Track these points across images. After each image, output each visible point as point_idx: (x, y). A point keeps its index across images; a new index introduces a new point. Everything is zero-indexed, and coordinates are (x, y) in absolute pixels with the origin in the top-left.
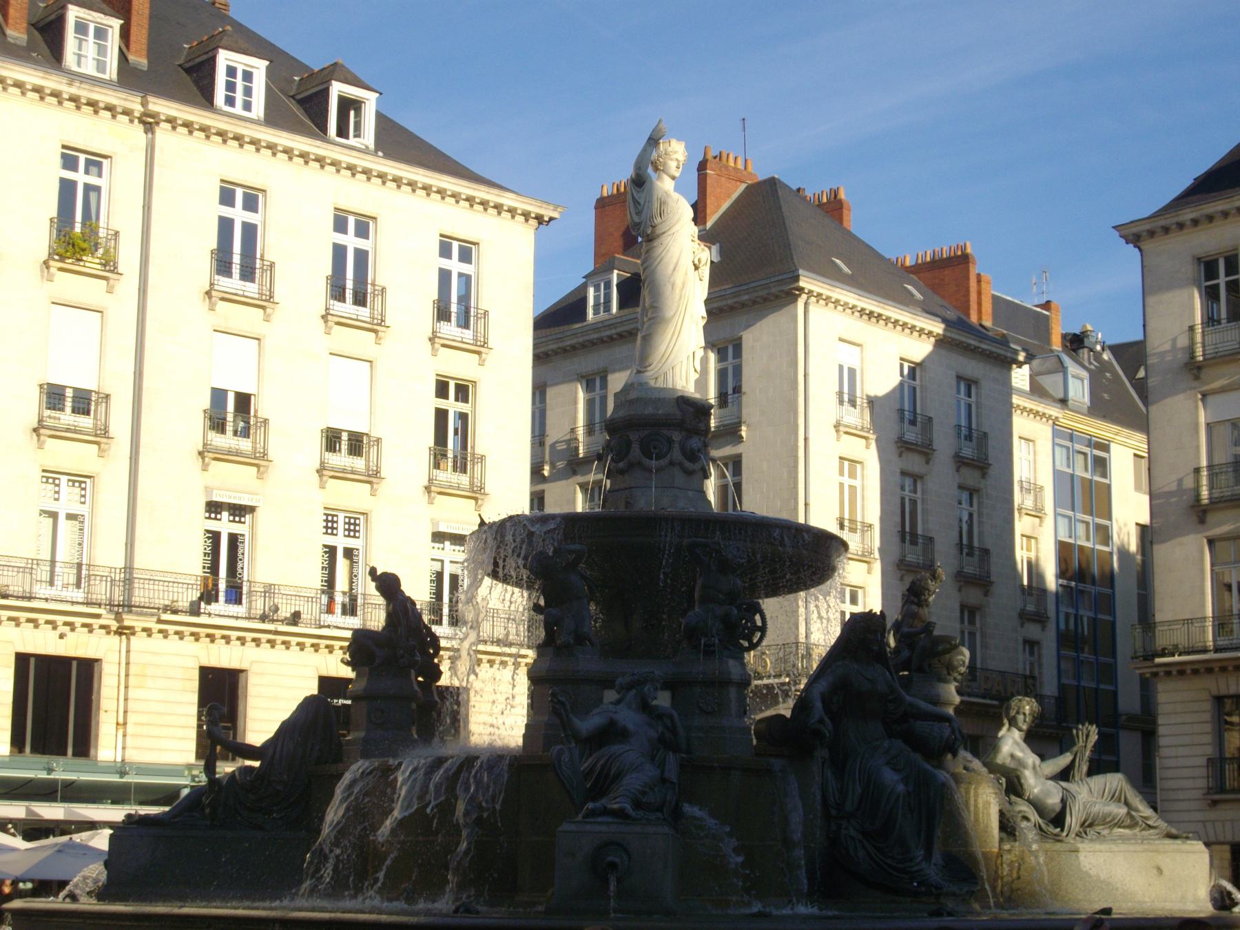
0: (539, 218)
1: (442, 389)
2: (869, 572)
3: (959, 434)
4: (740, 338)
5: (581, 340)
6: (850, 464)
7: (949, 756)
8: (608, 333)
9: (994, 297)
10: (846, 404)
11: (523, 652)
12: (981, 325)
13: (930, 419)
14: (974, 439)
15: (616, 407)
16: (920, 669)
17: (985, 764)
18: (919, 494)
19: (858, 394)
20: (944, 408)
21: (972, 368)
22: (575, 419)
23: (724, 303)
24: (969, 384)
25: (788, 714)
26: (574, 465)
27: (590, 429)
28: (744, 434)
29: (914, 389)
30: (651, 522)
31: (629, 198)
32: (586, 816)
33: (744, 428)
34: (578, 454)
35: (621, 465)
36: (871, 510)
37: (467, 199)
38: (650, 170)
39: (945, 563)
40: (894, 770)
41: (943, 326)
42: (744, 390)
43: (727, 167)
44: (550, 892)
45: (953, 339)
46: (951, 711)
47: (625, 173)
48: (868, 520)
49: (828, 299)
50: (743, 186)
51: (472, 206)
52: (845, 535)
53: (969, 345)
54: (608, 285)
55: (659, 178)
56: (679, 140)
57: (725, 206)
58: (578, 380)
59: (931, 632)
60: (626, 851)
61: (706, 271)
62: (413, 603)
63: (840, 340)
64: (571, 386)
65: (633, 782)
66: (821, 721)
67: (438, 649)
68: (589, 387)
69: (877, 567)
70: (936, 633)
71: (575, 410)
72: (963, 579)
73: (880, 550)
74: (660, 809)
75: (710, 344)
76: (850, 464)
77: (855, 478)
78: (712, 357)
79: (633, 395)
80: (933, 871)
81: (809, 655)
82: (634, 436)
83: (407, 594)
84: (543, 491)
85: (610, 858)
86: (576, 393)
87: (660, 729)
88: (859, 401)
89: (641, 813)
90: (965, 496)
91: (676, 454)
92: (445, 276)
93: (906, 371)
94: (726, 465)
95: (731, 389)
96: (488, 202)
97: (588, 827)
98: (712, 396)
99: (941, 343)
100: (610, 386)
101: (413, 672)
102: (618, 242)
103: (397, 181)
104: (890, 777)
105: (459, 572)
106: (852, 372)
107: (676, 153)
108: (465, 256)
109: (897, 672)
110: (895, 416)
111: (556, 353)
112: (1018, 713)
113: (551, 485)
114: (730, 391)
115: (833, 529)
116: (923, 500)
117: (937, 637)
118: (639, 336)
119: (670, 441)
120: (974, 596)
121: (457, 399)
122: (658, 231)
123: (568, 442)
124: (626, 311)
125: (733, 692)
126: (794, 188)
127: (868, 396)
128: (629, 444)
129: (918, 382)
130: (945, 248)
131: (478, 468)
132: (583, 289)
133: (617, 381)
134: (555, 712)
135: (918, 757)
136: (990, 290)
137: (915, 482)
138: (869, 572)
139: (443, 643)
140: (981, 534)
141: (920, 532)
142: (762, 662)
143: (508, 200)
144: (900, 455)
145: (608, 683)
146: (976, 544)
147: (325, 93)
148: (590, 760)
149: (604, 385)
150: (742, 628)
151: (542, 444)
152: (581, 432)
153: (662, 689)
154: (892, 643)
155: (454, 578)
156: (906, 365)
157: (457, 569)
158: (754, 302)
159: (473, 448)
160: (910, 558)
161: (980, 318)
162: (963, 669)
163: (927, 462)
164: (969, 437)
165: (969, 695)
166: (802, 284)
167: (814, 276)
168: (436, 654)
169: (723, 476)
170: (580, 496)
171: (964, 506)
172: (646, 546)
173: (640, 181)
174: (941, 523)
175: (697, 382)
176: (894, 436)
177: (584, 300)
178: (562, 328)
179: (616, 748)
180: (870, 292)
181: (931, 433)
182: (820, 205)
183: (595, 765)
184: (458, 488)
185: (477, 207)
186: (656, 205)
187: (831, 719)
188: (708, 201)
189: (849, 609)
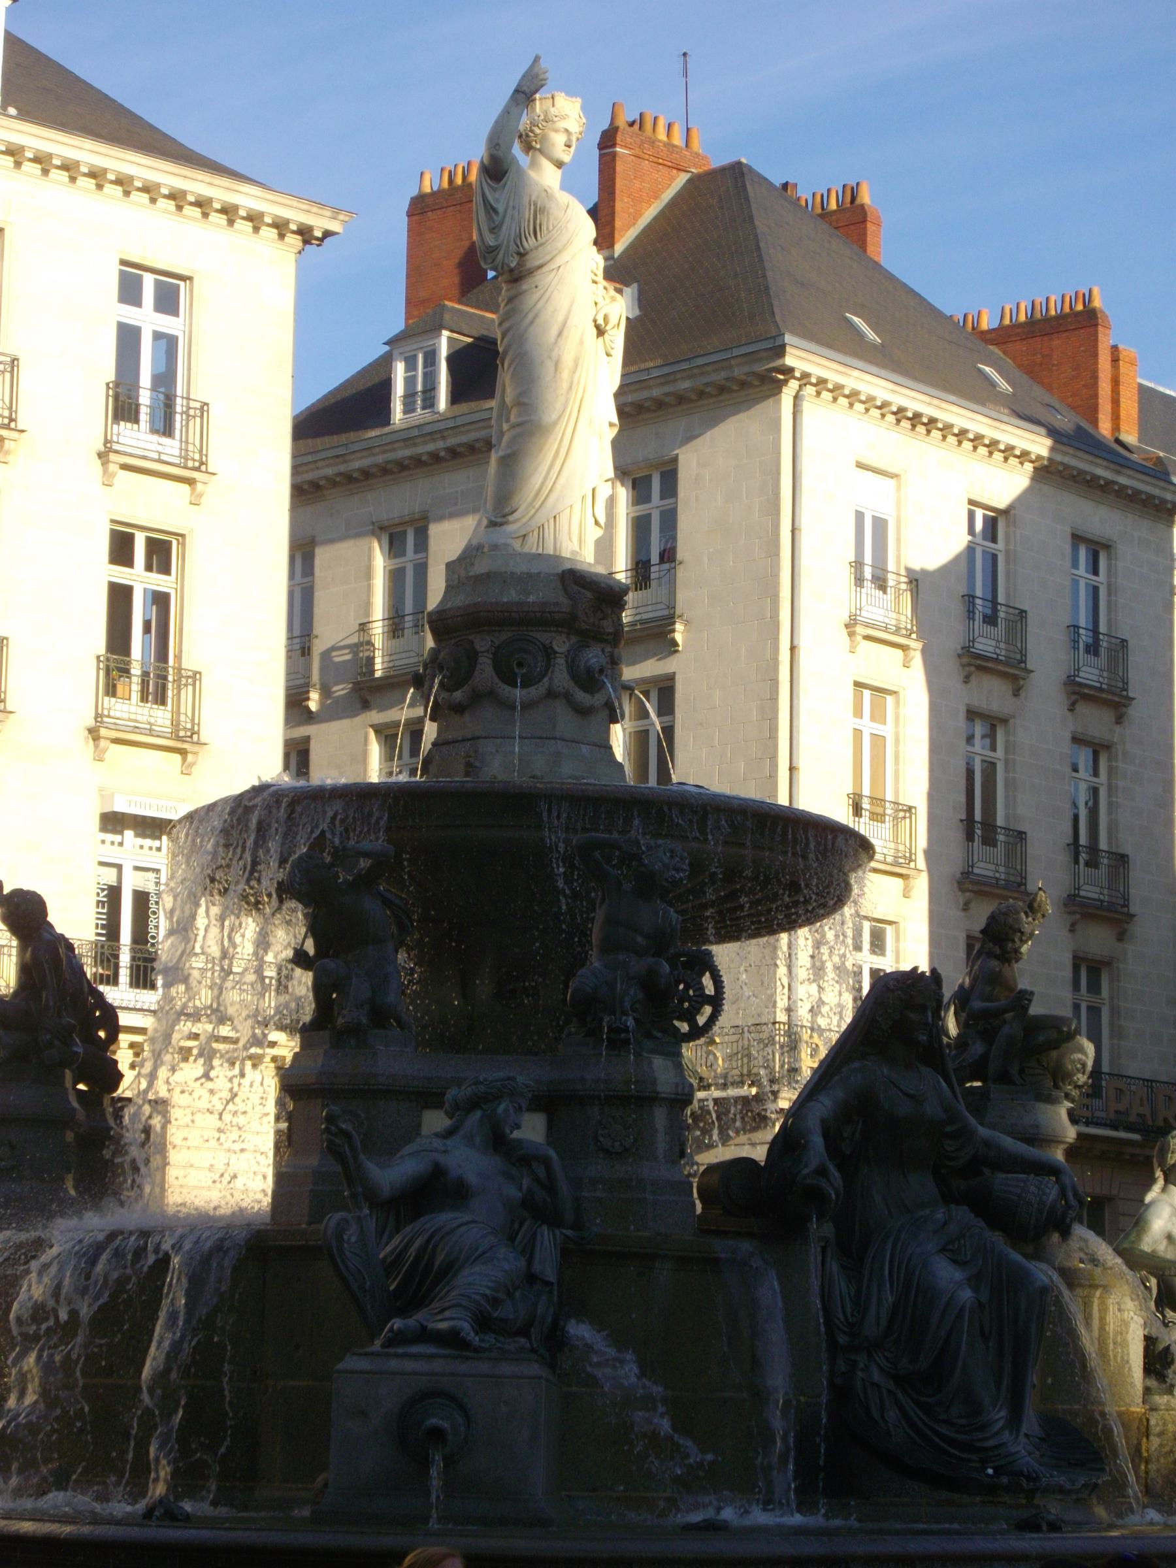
0: (305, 233)
1: (121, 548)
2: (906, 895)
3: (1075, 641)
4: (675, 460)
5: (380, 459)
6: (873, 695)
7: (1056, 1237)
8: (431, 447)
9: (1141, 388)
10: (867, 584)
11: (275, 1035)
12: (1118, 441)
13: (1022, 613)
14: (1102, 651)
15: (450, 589)
16: (1004, 1077)
17: (1119, 1252)
18: (1000, 752)
19: (891, 566)
20: (1049, 595)
21: (1101, 519)
22: (367, 606)
23: (645, 394)
24: (1095, 549)
25: (759, 1154)
26: (366, 692)
27: (395, 625)
28: (678, 637)
29: (994, 557)
30: (520, 803)
31: (477, 199)
32: (389, 1343)
33: (679, 627)
34: (373, 671)
35: (458, 695)
36: (912, 779)
37: (172, 196)
38: (517, 150)
39: (1048, 876)
40: (955, 1262)
41: (1048, 442)
42: (680, 555)
43: (653, 142)
44: (320, 1479)
45: (1067, 467)
46: (1059, 1155)
47: (476, 153)
48: (906, 800)
49: (837, 389)
50: (683, 178)
51: (180, 208)
52: (863, 826)
53: (1096, 478)
54: (431, 358)
55: (534, 164)
56: (570, 94)
57: (649, 214)
58: (373, 533)
59: (1025, 1009)
60: (462, 1407)
61: (617, 338)
62: (70, 947)
63: (860, 465)
64: (362, 542)
65: (476, 1280)
66: (822, 1171)
67: (114, 1030)
68: (395, 546)
69: (921, 884)
70: (1035, 1010)
71: (366, 587)
72: (1079, 909)
73: (928, 854)
74: (524, 1332)
75: (622, 472)
76: (873, 695)
77: (884, 722)
78: (623, 494)
79: (481, 567)
80: (1022, 1449)
81: (793, 1045)
82: (483, 643)
83: (59, 929)
84: (307, 739)
85: (434, 1421)
86: (370, 558)
87: (526, 1182)
88: (891, 580)
89: (490, 1339)
90: (1084, 757)
91: (560, 677)
92: (128, 337)
93: (979, 525)
94: (646, 694)
95: (656, 549)
96: (210, 201)
97: (394, 1364)
98: (621, 568)
99: (1045, 472)
100: (433, 546)
101: (68, 1075)
102: (450, 278)
103: (42, 160)
104: (947, 1274)
105: (151, 888)
106: (880, 525)
107: (567, 118)
108: (167, 301)
109: (961, 1083)
110: (957, 609)
111: (333, 483)
113: (323, 727)
114: (655, 559)
115: (841, 814)
116: (1007, 761)
117: (1037, 1018)
118: (494, 457)
119: (549, 653)
120: (1098, 940)
121: (149, 568)
122: (531, 262)
123: (355, 648)
124: (463, 408)
125: (660, 1116)
126: (778, 182)
127: (908, 570)
129: (1001, 545)
130: (1050, 292)
131: (187, 694)
132: (384, 364)
133: (450, 538)
134: (333, 1150)
135: (998, 1239)
136: (1136, 377)
137: (993, 727)
138: (906, 895)
139: (124, 1019)
140: (1112, 828)
141: (1000, 822)
142: (710, 1061)
143: (247, 198)
144: (967, 679)
145: (430, 1098)
146: (1103, 845)
148: (395, 1241)
149: (422, 543)
150: (677, 998)
151: (306, 651)
152: (378, 631)
153: (529, 1110)
154: (952, 1026)
155: (142, 900)
156: (979, 514)
157: (145, 882)
158: (701, 394)
159: (178, 657)
160: (983, 869)
161: (1116, 428)
162: (1082, 1079)
163: (1016, 693)
164: (1093, 649)
165: (1087, 1124)
166: (789, 361)
167: (813, 346)
168: (113, 1038)
169: (643, 714)
170: (375, 750)
171: (1082, 774)
172: (499, 852)
173: (497, 169)
174: (1040, 808)
175: (598, 543)
176: (954, 643)
177: (386, 385)
178: (343, 438)
179: (444, 1218)
180: (915, 378)
181: (1024, 640)
182: (825, 215)
184: (151, 732)
185: (189, 210)
186: (528, 214)
187: (839, 1167)
188: (619, 205)
189: (868, 961)
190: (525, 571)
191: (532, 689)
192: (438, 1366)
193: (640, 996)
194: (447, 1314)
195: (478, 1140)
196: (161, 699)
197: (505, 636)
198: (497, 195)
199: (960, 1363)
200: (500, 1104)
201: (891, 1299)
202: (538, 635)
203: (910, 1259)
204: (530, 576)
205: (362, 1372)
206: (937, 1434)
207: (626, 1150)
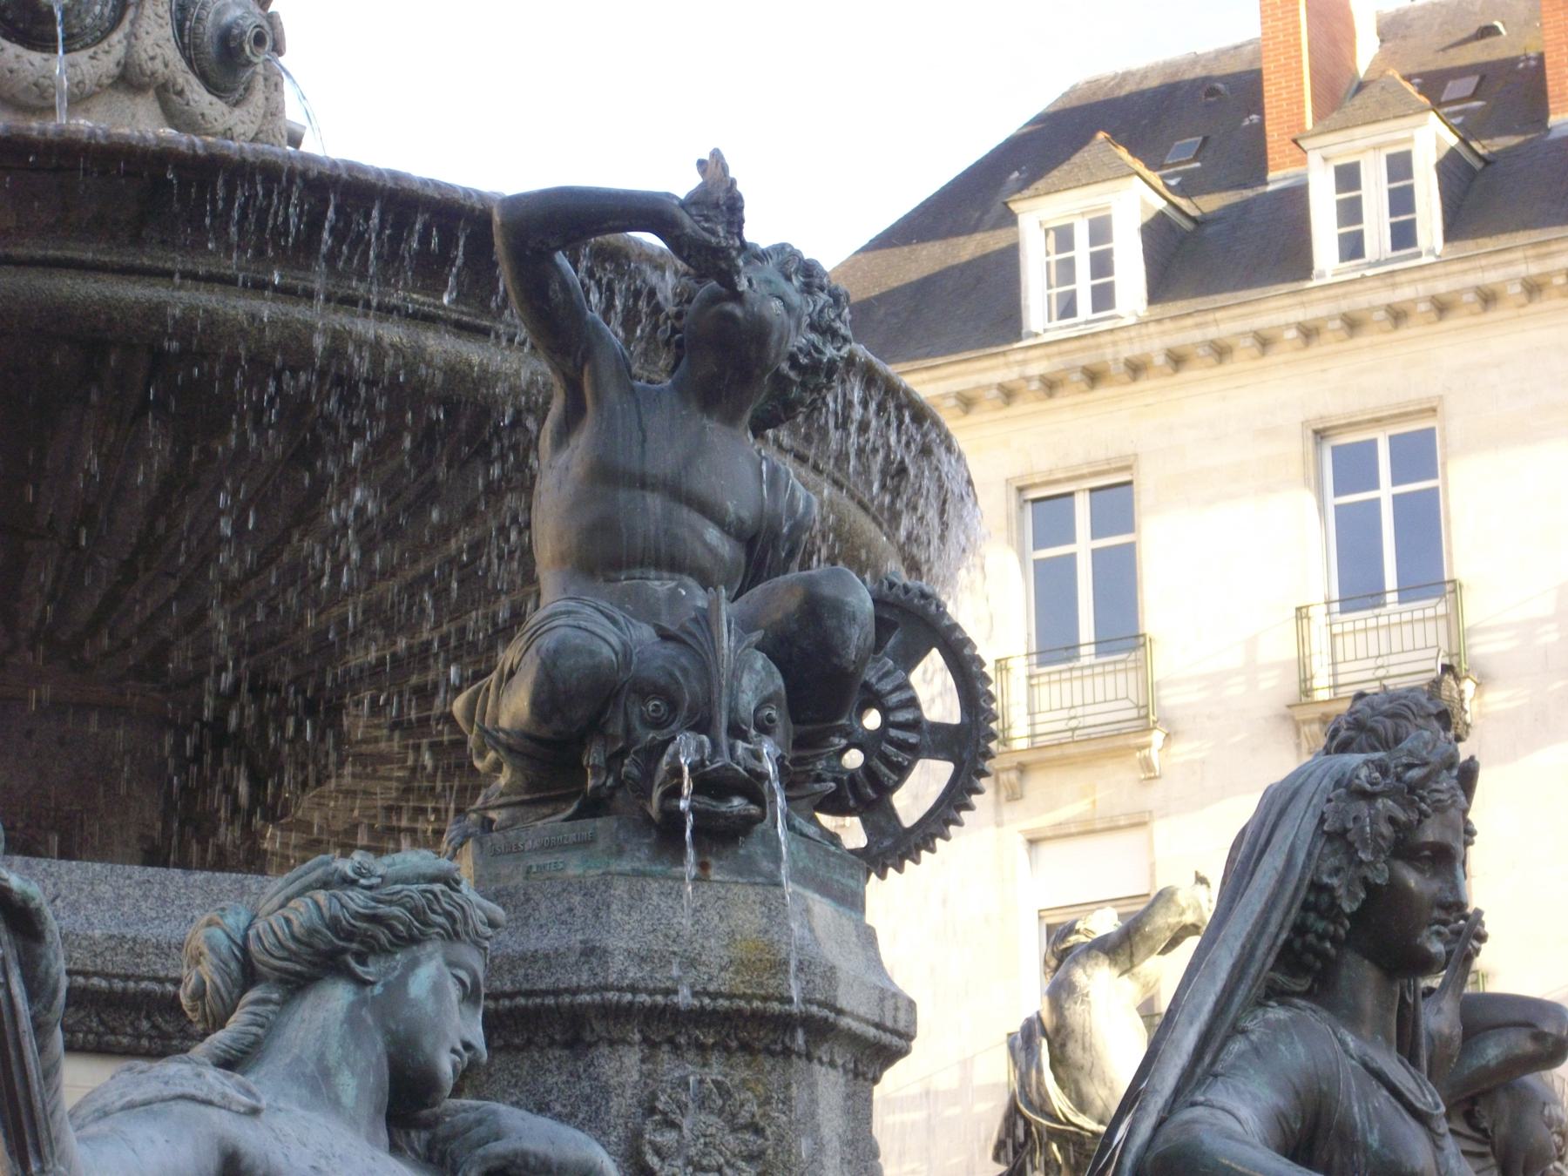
191: (82, 57)
195: (348, 1086)
200: (414, 964)
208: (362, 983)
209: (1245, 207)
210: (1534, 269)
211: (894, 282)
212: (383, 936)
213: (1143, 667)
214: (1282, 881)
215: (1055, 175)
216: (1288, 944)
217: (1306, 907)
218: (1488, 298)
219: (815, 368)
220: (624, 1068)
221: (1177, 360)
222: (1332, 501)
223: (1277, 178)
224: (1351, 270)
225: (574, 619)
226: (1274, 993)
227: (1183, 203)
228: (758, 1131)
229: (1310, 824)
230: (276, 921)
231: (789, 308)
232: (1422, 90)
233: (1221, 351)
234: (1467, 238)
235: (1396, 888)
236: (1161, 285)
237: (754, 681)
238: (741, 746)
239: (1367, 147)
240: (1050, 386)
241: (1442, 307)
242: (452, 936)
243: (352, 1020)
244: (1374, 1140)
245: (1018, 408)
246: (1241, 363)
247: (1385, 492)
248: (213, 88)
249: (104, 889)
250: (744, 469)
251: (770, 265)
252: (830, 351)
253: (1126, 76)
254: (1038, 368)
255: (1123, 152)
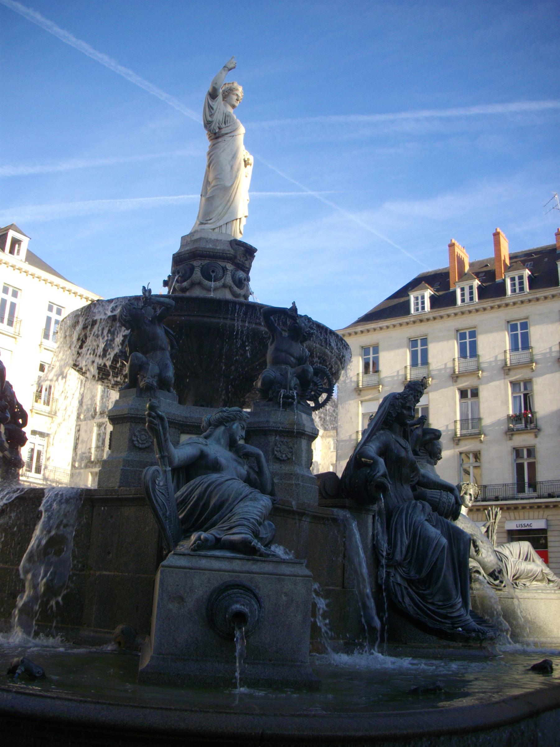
35: (185, 284)
85: (237, 607)
91: (228, 279)
97: (204, 563)
112: (466, 493)
119: (224, 269)
128: (192, 269)
147: (5, 236)
157: (40, 448)
183: (191, 493)
190: (216, 238)
191: (217, 283)
192: (237, 565)
193: (298, 382)
194: (234, 530)
195: (222, 441)
196: (48, 404)
197: (206, 262)
198: (214, 103)
199: (443, 575)
200: (234, 424)
201: (407, 542)
202: (220, 263)
203: (415, 523)
204: (217, 240)
205: (181, 567)
206: (428, 609)
207: (288, 459)
208: (226, 426)
209: (446, 293)
210: (492, 305)
211: (390, 305)
212: (229, 419)
213: (428, 368)
214: (383, 412)
215: (416, 289)
216: (384, 421)
217: (387, 415)
218: (485, 309)
219: (309, 333)
220: (272, 439)
221: (435, 318)
222: (459, 342)
223: (452, 289)
224: (463, 304)
225: (270, 371)
226: (383, 429)
227: (436, 293)
228: (292, 448)
229: (388, 403)
230: (214, 417)
231: (305, 325)
232: (476, 275)
233: (442, 317)
234: (488, 298)
235: (402, 414)
236: (433, 306)
237: (294, 381)
238: (291, 391)
239: (466, 284)
240: (414, 322)
241: (477, 311)
242: (240, 420)
243: (224, 432)
244: (396, 451)
245: (409, 326)
246: (445, 319)
247: (468, 340)
248: (238, 287)
249: (198, 411)
250: (300, 349)
251: (303, 319)
252: (312, 331)
253: (428, 272)
254: (412, 319)
255: (427, 285)
